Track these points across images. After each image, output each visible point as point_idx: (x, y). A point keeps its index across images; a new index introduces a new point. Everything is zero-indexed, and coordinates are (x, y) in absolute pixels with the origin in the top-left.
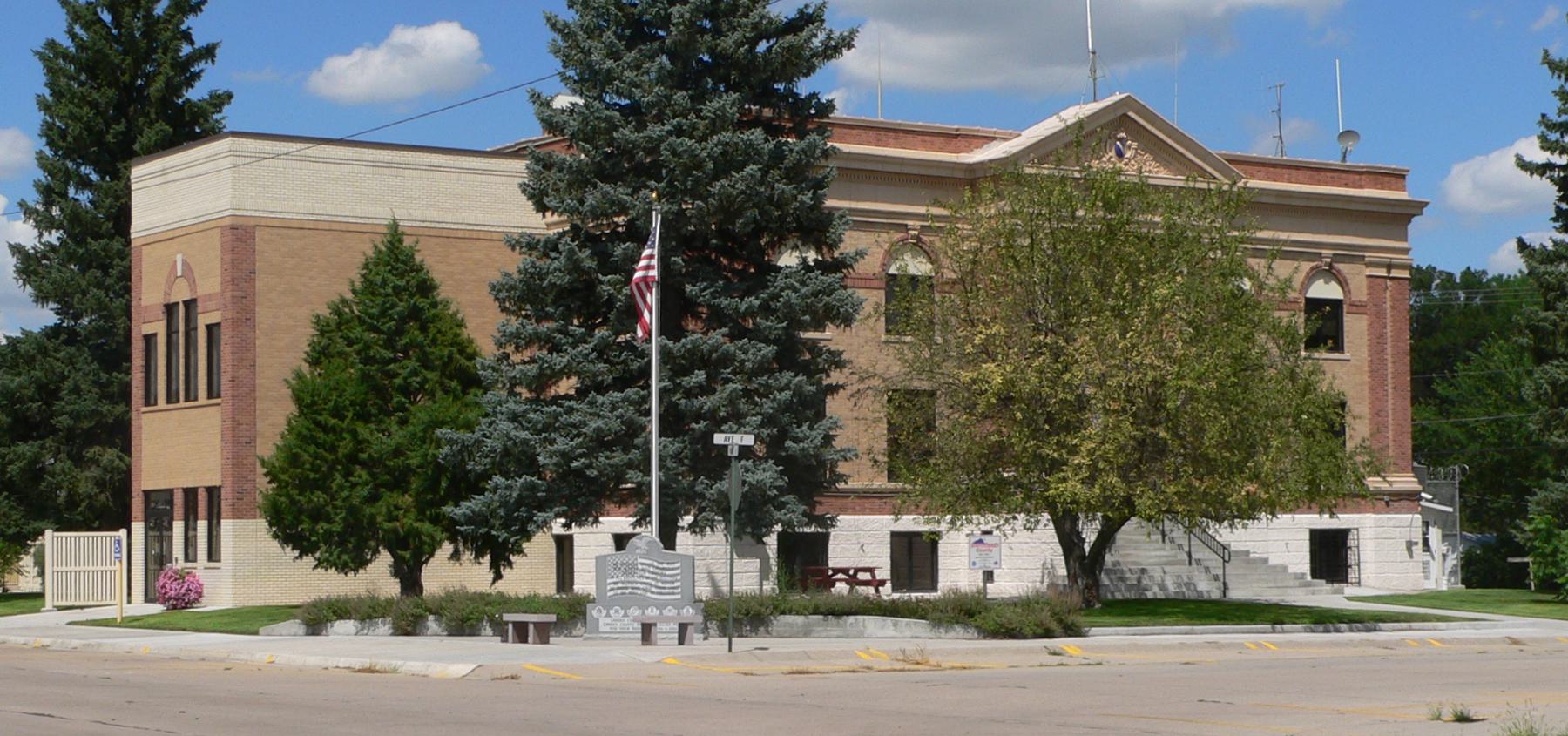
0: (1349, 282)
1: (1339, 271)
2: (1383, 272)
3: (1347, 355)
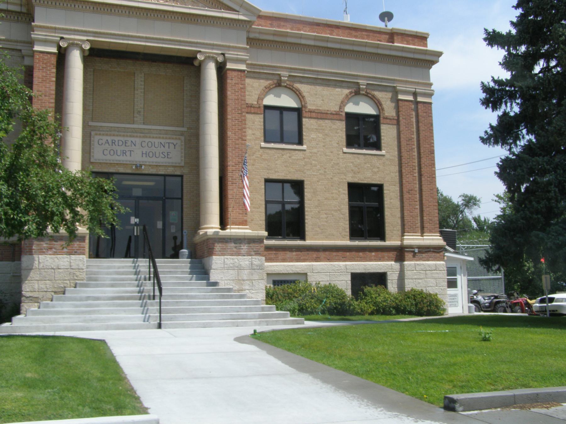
0: (383, 103)
1: (373, 96)
2: (411, 98)
3: (383, 152)
